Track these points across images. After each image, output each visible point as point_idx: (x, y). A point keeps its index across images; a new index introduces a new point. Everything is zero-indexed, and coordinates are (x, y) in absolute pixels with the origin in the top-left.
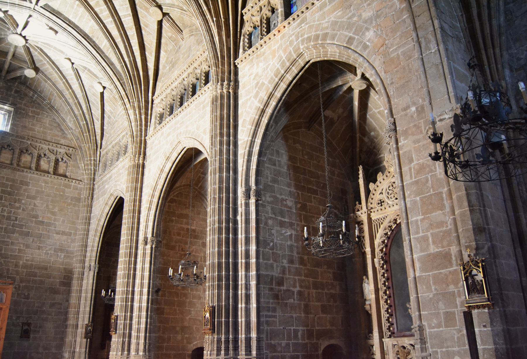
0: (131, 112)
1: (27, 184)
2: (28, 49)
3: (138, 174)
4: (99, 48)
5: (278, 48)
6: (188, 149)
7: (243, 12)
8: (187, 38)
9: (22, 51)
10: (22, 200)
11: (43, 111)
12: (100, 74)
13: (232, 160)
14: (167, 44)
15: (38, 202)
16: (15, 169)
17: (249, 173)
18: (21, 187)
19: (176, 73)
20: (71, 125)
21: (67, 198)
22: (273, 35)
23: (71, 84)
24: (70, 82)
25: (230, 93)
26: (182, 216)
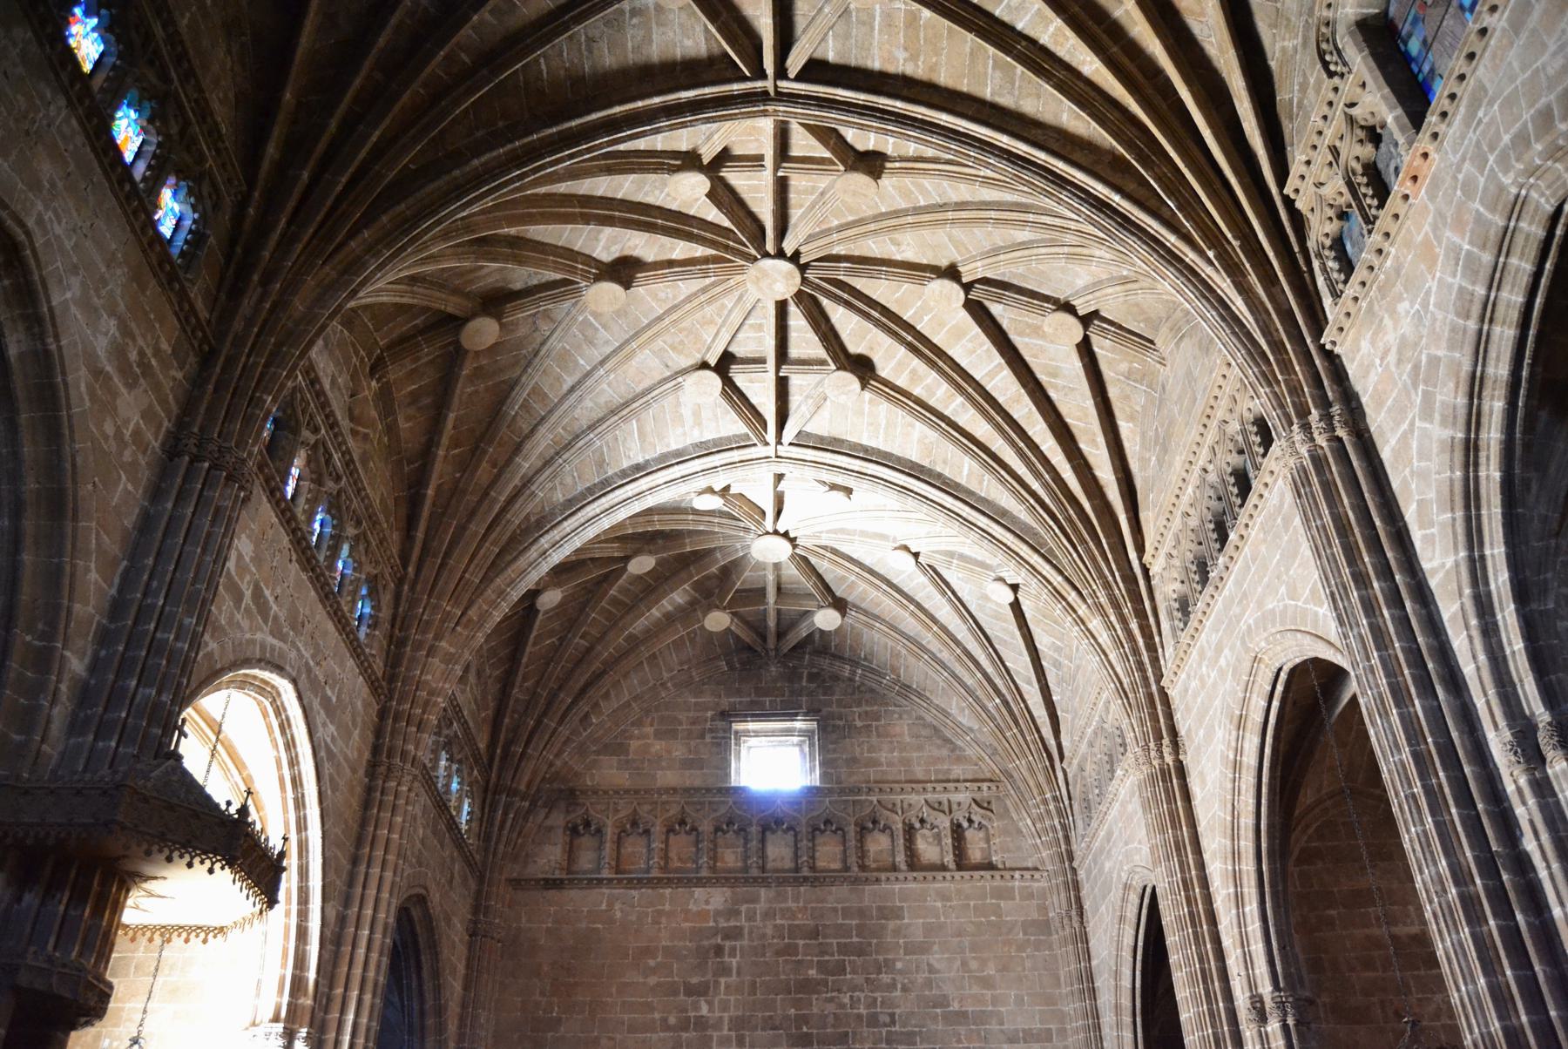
0: (1095, 624)
1: (897, 914)
2: (804, 563)
3: (1170, 799)
4: (957, 486)
5: (1435, 228)
6: (1292, 672)
7: (1288, 190)
8: (1171, 352)
9: (792, 572)
10: (894, 961)
11: (887, 704)
12: (995, 558)
13: (1430, 649)
14: (1127, 398)
15: (936, 958)
16: (856, 881)
17: (1508, 673)
18: (883, 927)
19: (1178, 461)
20: (966, 719)
21: (1010, 931)
22: (1399, 200)
23: (932, 611)
24: (926, 606)
25: (1340, 440)
26: (1361, 898)
